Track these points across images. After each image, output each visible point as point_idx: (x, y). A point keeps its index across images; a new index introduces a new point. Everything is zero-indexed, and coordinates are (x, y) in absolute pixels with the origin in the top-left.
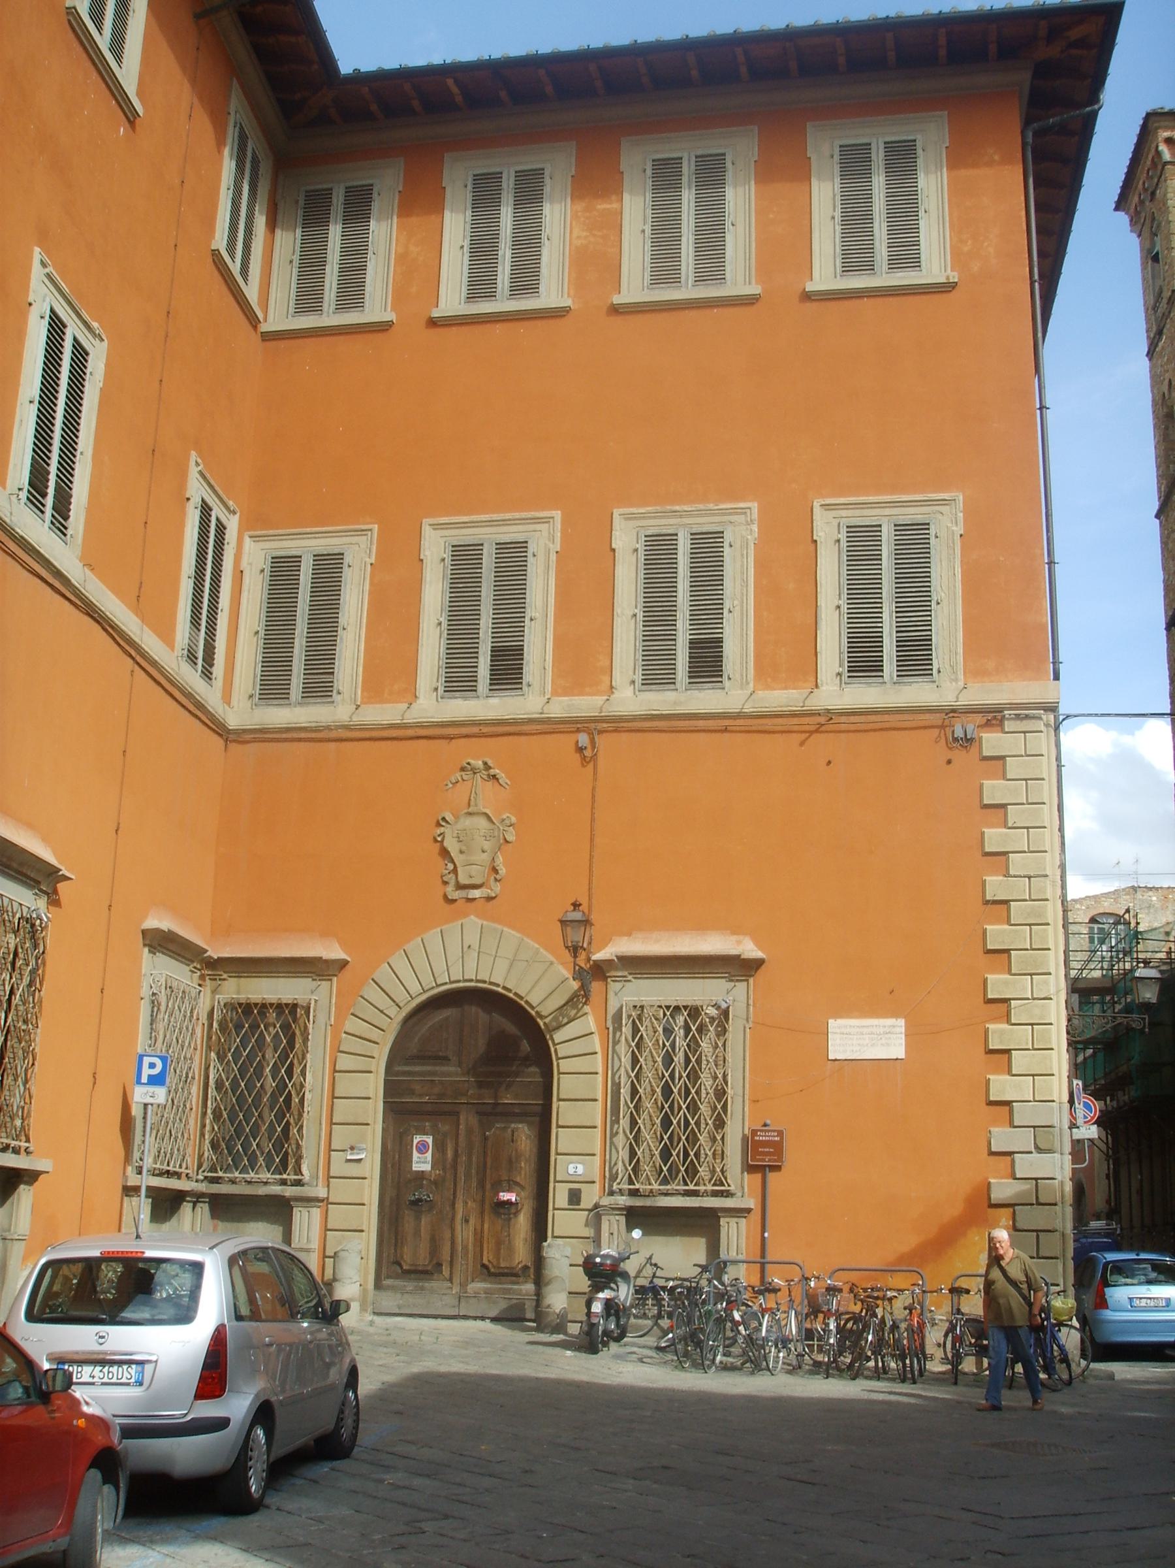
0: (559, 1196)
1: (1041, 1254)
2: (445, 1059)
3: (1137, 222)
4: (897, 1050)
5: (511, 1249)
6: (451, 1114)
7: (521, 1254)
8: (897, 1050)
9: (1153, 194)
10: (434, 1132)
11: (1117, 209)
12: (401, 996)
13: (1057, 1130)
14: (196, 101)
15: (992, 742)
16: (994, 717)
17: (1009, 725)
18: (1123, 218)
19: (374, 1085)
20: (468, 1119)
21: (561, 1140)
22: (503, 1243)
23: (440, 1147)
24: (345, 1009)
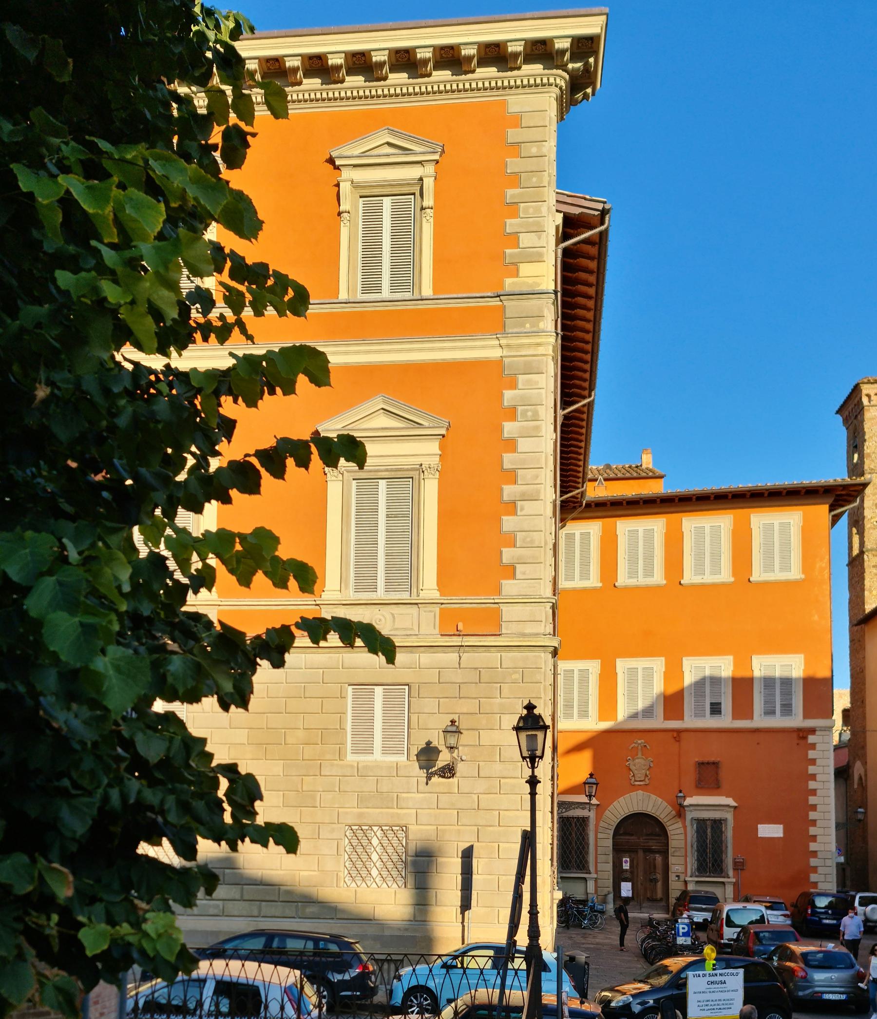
0: (672, 877)
1: (307, 695)
2: (632, 835)
3: (846, 421)
5: (656, 892)
6: (635, 851)
7: (659, 894)
9: (856, 416)
10: (630, 857)
11: (837, 412)
12: (673, 837)
13: (543, 670)
14: (213, 134)
15: (811, 739)
16: (813, 731)
17: (817, 733)
18: (839, 419)
19: (609, 843)
20: (641, 854)
21: (672, 860)
22: (654, 890)
24: (599, 818)
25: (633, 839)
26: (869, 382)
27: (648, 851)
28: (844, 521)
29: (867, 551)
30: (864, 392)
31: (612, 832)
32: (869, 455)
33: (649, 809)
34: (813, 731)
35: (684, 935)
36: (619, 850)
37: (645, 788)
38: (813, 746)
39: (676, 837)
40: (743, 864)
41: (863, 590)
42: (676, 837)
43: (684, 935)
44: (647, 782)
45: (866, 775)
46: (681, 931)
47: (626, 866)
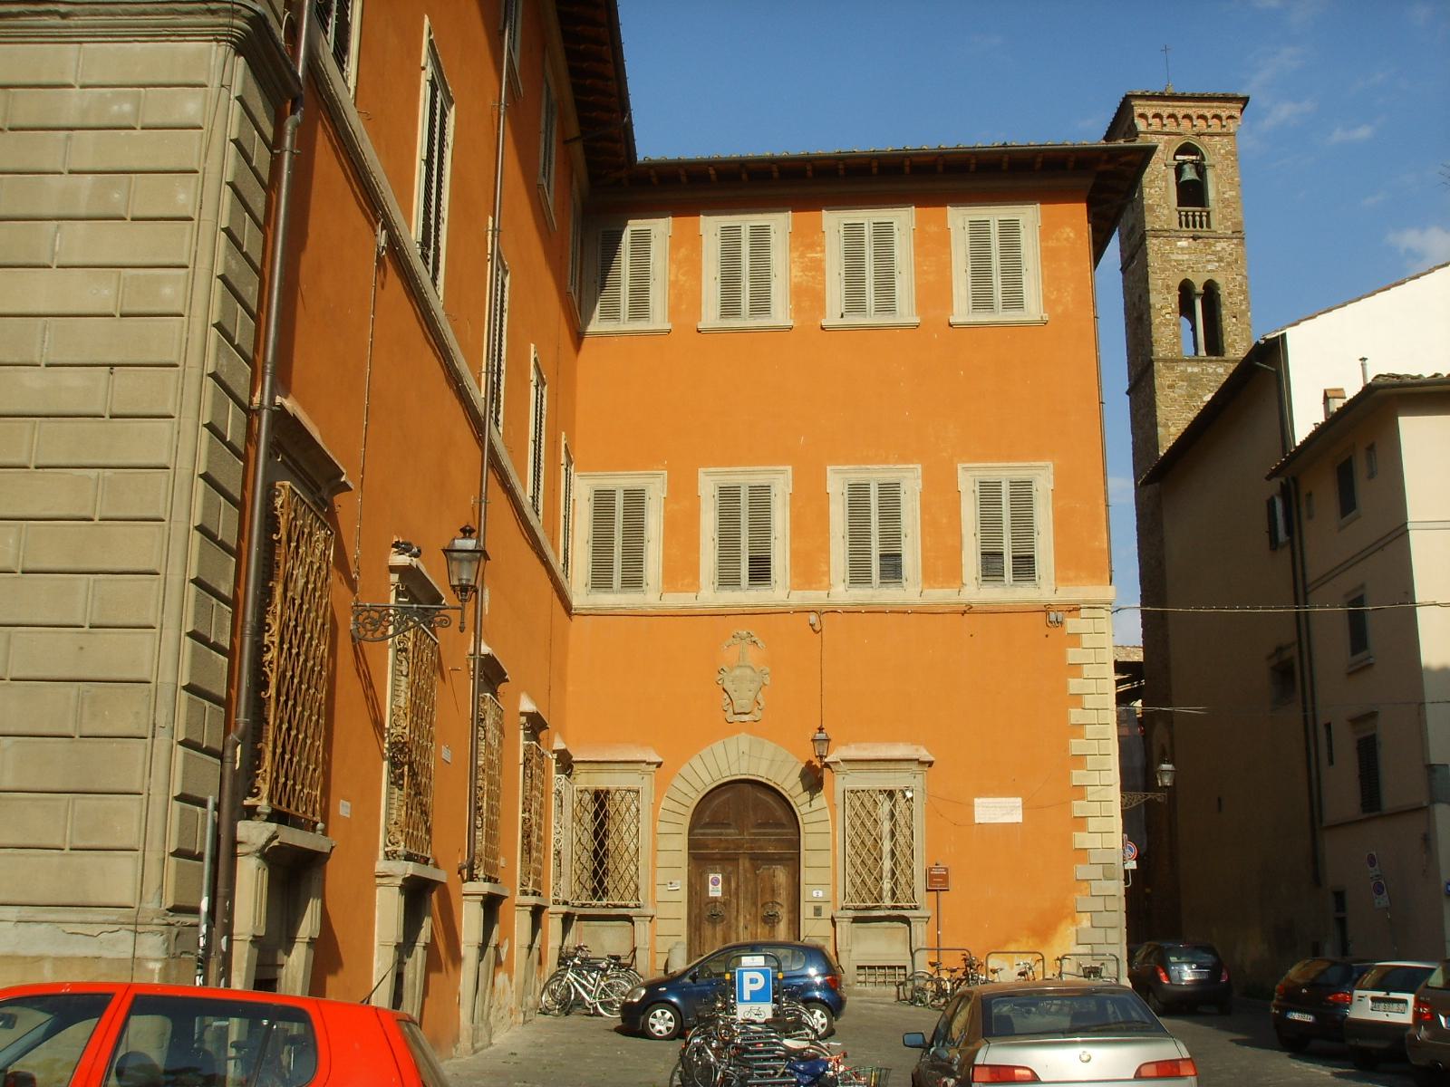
0: (807, 911)
2: (728, 825)
4: (1017, 817)
8: (1017, 817)
10: (723, 872)
15: (1072, 624)
16: (1074, 609)
19: (681, 842)
20: (744, 864)
21: (806, 876)
23: (727, 881)
25: (731, 833)
26: (1143, 97)
27: (759, 859)
28: (1114, 249)
29: (1158, 360)
30: (1138, 111)
31: (686, 821)
32: (1151, 208)
33: (761, 772)
34: (1074, 609)
35: (755, 997)
36: (700, 858)
37: (754, 728)
38: (1075, 639)
39: (815, 828)
40: (945, 878)
41: (1155, 425)
42: (815, 828)
43: (755, 997)
44: (758, 715)
45: (1172, 745)
46: (748, 988)
47: (715, 891)
